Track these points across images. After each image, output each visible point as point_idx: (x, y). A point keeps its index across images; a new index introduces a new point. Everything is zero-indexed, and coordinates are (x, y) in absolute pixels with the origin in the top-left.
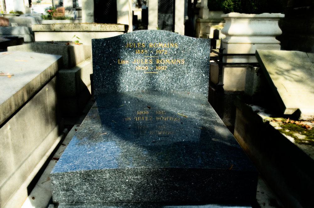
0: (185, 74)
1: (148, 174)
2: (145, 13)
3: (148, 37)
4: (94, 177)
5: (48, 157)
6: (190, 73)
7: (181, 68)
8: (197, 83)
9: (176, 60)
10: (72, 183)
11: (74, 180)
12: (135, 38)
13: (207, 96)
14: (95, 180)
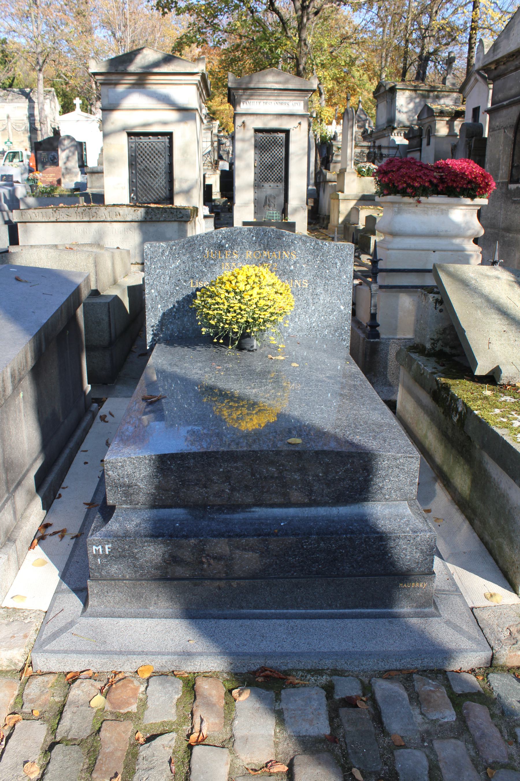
0: (308, 305)
1: (253, 461)
2: (228, 180)
3: (244, 241)
4: (171, 465)
5: (463, 331)
6: (318, 305)
7: (302, 295)
8: (330, 322)
9: (294, 281)
10: (137, 474)
11: (140, 470)
12: (221, 241)
13: (348, 344)
14: (172, 469)
